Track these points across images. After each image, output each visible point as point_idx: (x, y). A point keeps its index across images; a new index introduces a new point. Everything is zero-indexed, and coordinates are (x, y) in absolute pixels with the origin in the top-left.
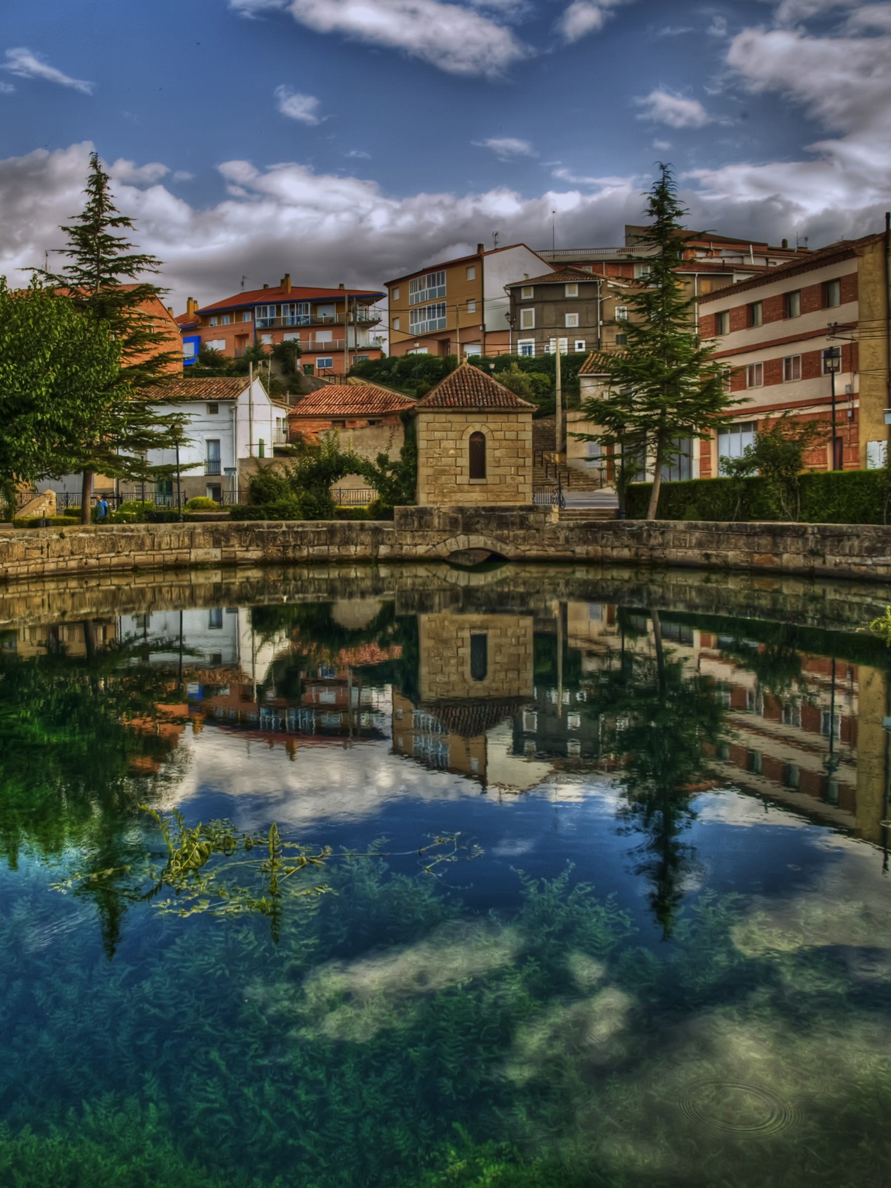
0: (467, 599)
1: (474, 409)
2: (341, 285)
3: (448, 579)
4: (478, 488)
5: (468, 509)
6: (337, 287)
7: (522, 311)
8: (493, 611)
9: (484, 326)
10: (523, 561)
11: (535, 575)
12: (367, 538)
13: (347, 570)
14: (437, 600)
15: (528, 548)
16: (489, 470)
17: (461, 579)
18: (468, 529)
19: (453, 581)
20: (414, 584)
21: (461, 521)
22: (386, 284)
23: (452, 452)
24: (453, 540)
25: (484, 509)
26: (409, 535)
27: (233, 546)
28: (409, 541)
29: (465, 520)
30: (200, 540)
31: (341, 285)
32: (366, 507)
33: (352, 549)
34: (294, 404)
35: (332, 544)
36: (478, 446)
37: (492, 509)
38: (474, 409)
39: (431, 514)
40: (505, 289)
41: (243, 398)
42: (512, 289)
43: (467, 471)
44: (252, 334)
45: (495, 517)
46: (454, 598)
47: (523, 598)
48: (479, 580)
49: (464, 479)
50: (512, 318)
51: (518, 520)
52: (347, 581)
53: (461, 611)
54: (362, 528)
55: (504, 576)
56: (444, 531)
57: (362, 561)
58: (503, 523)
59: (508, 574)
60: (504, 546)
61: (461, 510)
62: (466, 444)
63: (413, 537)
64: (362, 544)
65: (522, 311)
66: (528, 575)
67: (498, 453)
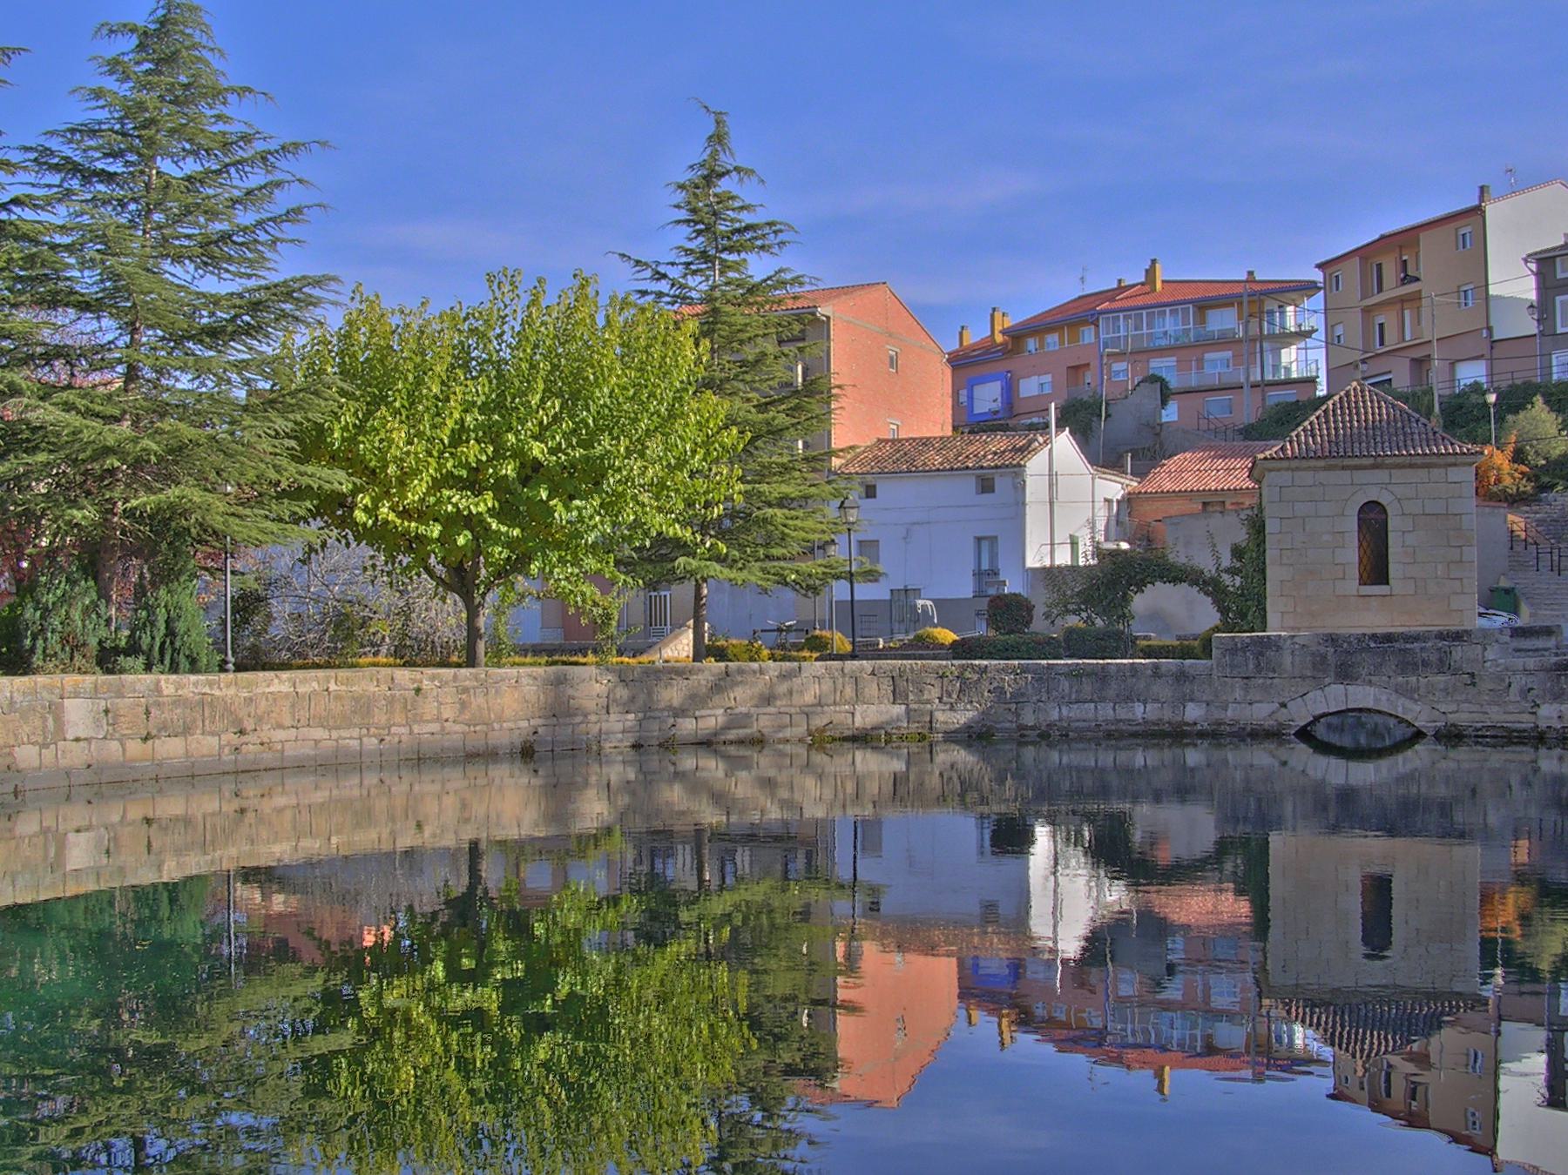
0: (1344, 811)
1: (1365, 461)
2: (1251, 273)
3: (1310, 772)
4: (1374, 602)
5: (1347, 639)
6: (1244, 277)
7: (1558, 299)
8: (1392, 832)
9: (1489, 329)
10: (1451, 736)
11: (1465, 766)
12: (1163, 690)
13: (1130, 753)
14: (1288, 808)
15: (1453, 707)
16: (1394, 570)
17: (1335, 772)
18: (1345, 675)
19: (1319, 775)
20: (1247, 781)
21: (1331, 659)
22: (1319, 266)
23: (1325, 538)
24: (1319, 692)
25: (1374, 637)
26: (1239, 683)
27: (928, 702)
28: (1238, 694)
29: (1341, 657)
30: (871, 689)
31: (1251, 273)
32: (1196, 643)
33: (1139, 709)
34: (1140, 473)
35: (1103, 700)
36: (1373, 521)
37: (1389, 638)
38: (1365, 461)
39: (1279, 648)
40: (1526, 261)
41: (1035, 465)
42: (1539, 261)
43: (1354, 572)
44: (1094, 364)
45: (1390, 649)
46: (1320, 805)
47: (1445, 808)
48: (1364, 774)
49: (1352, 585)
50: (1541, 313)
51: (1434, 658)
52: (1128, 772)
53: (1334, 829)
54: (1156, 672)
55: (1409, 767)
56: (1303, 678)
57: (1152, 735)
58: (1408, 665)
59: (1417, 763)
60: (1409, 704)
61: (1332, 639)
62: (1352, 524)
63: (1246, 689)
64: (1156, 700)
65: (1558, 299)
66: (1453, 765)
67: (1410, 539)
